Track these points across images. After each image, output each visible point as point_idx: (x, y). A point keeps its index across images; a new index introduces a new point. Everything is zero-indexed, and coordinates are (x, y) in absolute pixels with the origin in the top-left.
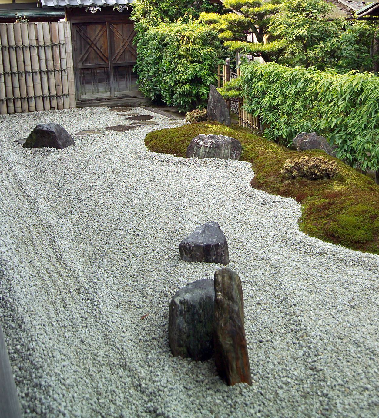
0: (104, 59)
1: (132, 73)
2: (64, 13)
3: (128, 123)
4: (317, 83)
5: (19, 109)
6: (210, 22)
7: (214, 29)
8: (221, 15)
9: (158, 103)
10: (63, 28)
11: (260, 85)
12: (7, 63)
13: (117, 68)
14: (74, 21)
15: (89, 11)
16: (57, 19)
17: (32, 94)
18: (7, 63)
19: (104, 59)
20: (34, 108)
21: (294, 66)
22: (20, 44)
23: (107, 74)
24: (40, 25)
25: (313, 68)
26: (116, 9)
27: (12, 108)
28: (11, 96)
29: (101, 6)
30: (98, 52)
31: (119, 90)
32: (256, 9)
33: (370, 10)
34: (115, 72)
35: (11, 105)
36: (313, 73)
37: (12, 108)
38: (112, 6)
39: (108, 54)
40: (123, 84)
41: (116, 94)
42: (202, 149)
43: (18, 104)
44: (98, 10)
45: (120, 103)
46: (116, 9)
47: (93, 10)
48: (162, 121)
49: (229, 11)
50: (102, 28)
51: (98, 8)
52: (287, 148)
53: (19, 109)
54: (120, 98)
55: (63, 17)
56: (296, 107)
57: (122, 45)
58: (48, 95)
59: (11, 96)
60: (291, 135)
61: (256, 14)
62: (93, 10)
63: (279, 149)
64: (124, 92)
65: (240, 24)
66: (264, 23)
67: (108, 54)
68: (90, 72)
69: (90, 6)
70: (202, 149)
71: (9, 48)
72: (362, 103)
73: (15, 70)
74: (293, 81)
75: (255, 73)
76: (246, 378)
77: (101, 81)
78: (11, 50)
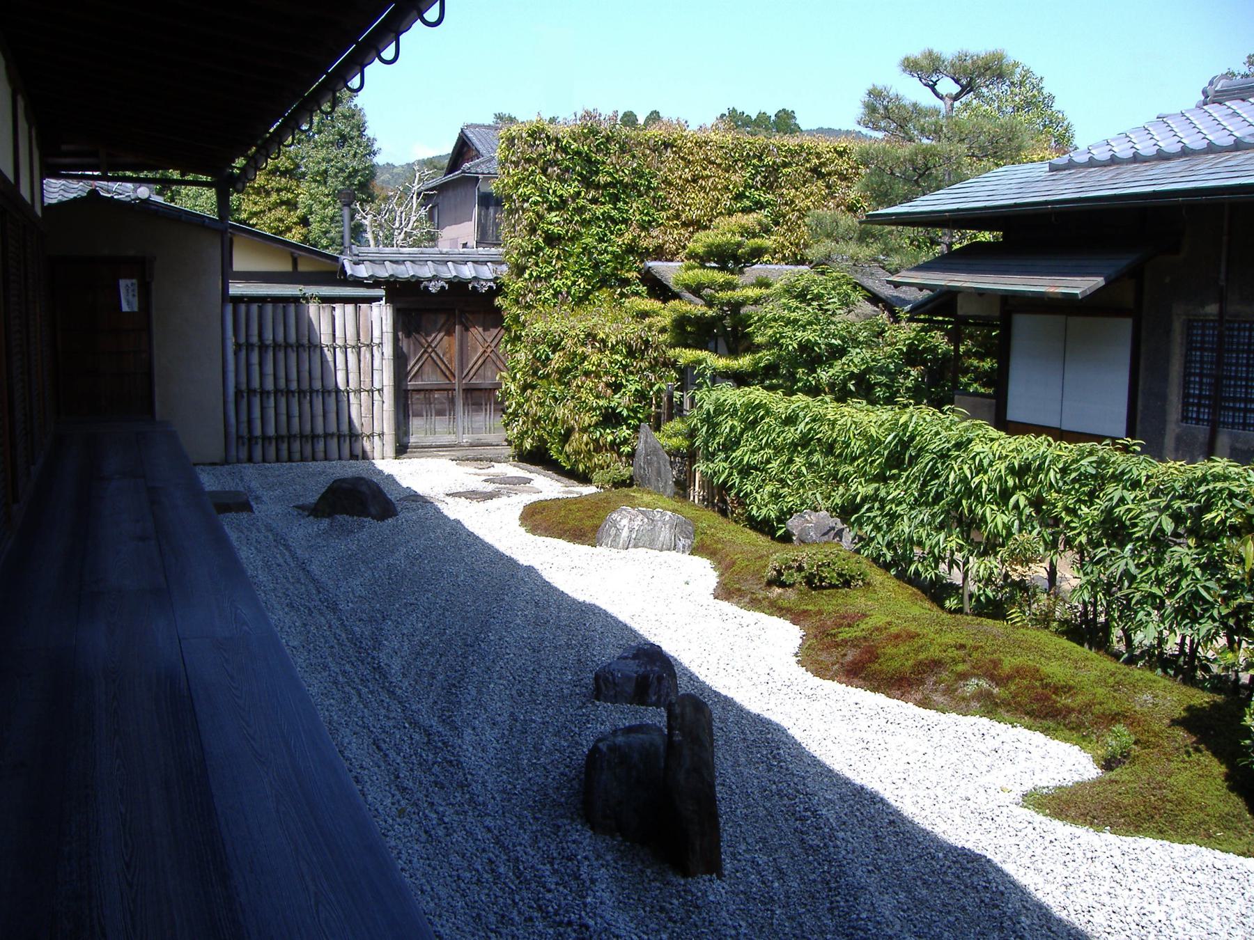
0: (448, 374)
1: (496, 403)
2: (381, 292)
3: (490, 487)
4: (834, 423)
5: (297, 456)
6: (644, 315)
7: (650, 327)
8: (664, 302)
9: (538, 457)
10: (380, 316)
11: (727, 425)
12: (282, 374)
13: (469, 391)
14: (399, 305)
15: (426, 288)
16: (370, 300)
17: (320, 430)
18: (282, 374)
19: (448, 374)
20: (321, 455)
21: (793, 393)
22: (305, 341)
23: (452, 401)
24: (338, 306)
25: (827, 398)
26: (474, 287)
27: (285, 453)
28: (284, 431)
29: (449, 282)
30: (439, 362)
31: (474, 431)
32: (729, 294)
33: (929, 306)
34: (465, 399)
35: (285, 446)
36: (828, 407)
37: (285, 453)
38: (470, 281)
39: (455, 366)
40: (480, 419)
41: (466, 439)
42: (625, 533)
43: (296, 446)
44: (443, 287)
45: (471, 453)
46: (474, 287)
47: (434, 288)
48: (548, 487)
49: (676, 296)
50: (447, 320)
51: (443, 283)
52: (773, 538)
53: (297, 456)
54: (472, 445)
55: (378, 299)
56: (794, 468)
57: (481, 350)
58: (347, 432)
59: (284, 431)
60: (783, 517)
61: (729, 303)
62: (434, 288)
63: (762, 541)
64: (480, 436)
65: (699, 321)
66: (741, 319)
67: (455, 366)
68: (421, 396)
69: (430, 280)
70: (625, 533)
71: (286, 348)
72: (913, 460)
73: (294, 386)
74: (791, 420)
75: (722, 404)
76: (714, 867)
77: (440, 413)
78: (290, 350)
